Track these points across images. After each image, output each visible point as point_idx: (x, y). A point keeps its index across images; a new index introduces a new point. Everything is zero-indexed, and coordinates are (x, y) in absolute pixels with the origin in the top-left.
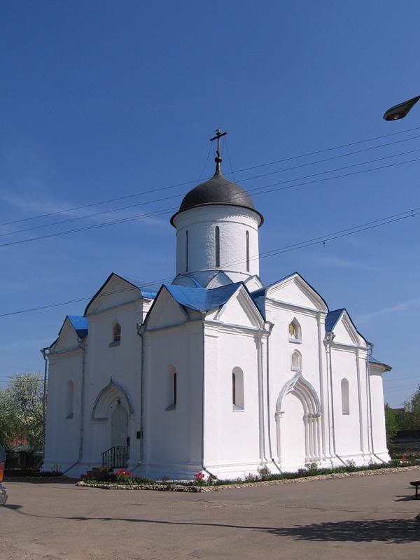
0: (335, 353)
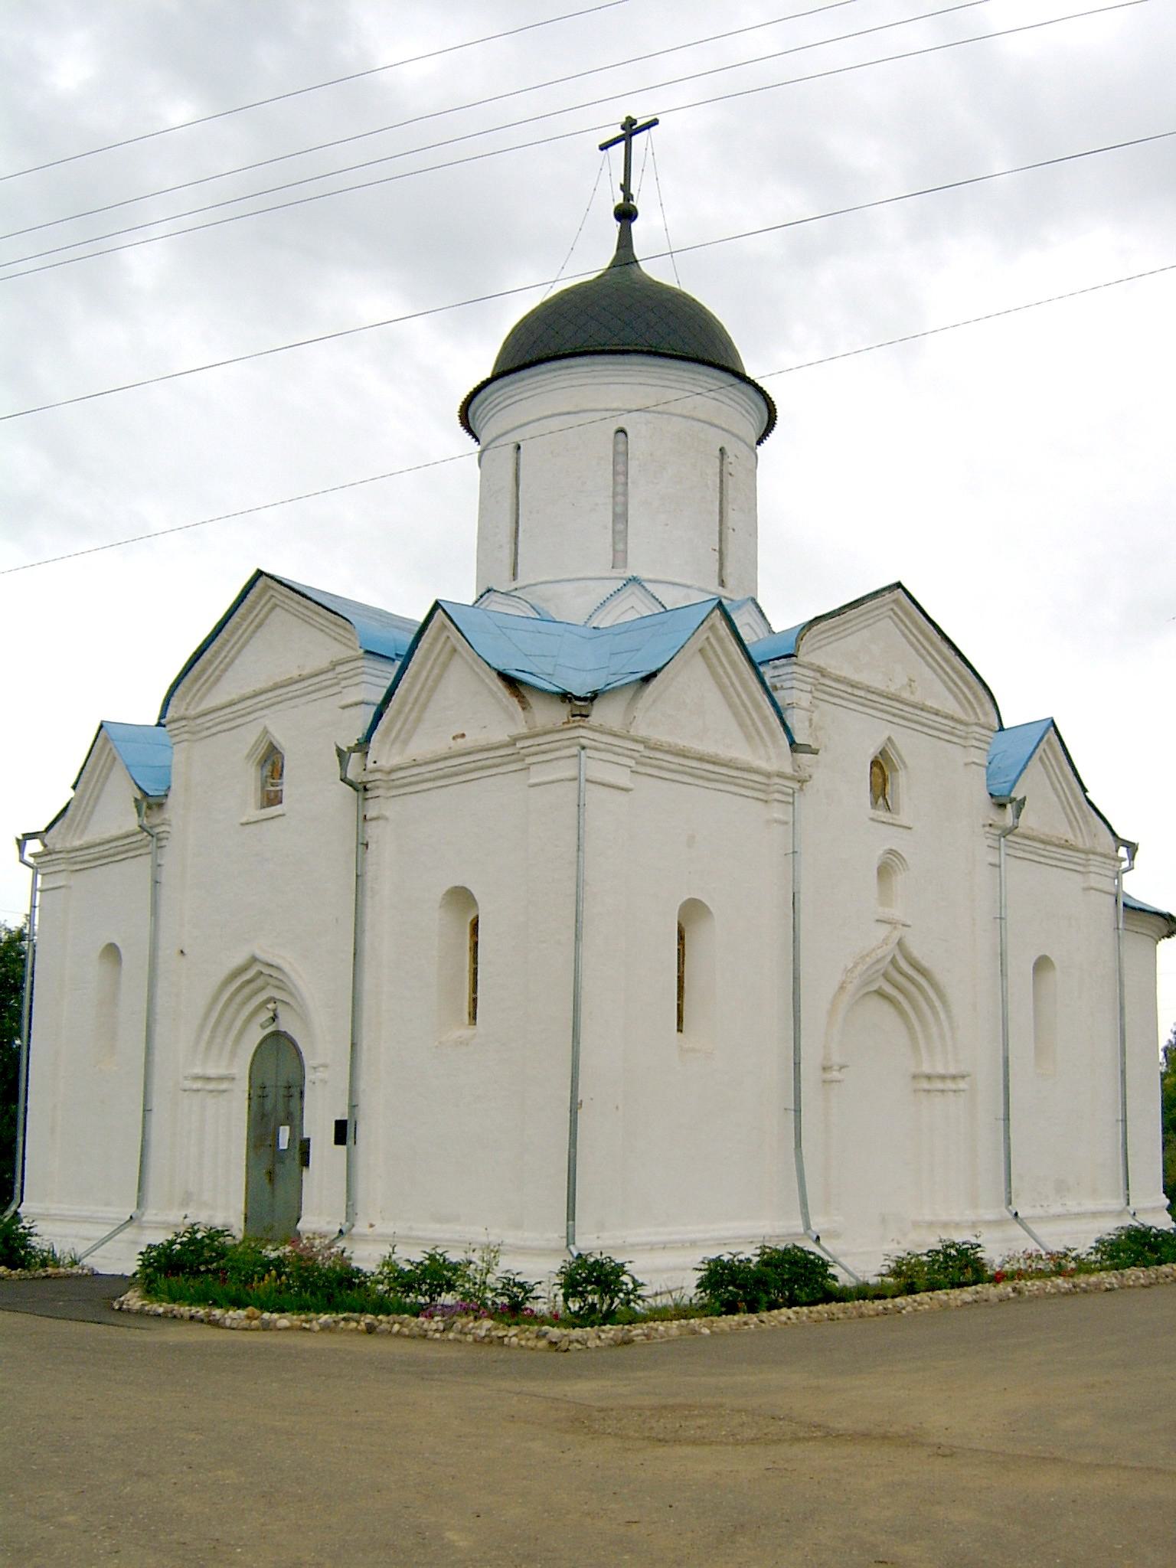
0: (1022, 875)
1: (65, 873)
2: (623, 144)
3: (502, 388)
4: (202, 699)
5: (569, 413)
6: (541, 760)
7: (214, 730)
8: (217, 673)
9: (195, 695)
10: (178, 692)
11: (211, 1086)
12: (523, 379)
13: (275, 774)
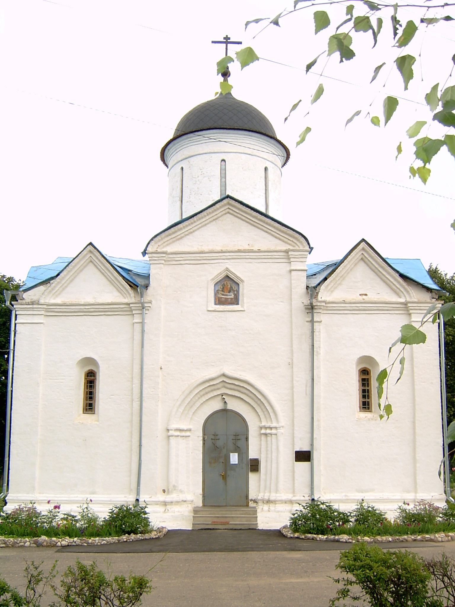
1: (43, 316)
4: (166, 246)
5: (249, 154)
6: (419, 312)
8: (183, 235)
9: (164, 242)
10: (156, 239)
11: (183, 434)
13: (225, 289)
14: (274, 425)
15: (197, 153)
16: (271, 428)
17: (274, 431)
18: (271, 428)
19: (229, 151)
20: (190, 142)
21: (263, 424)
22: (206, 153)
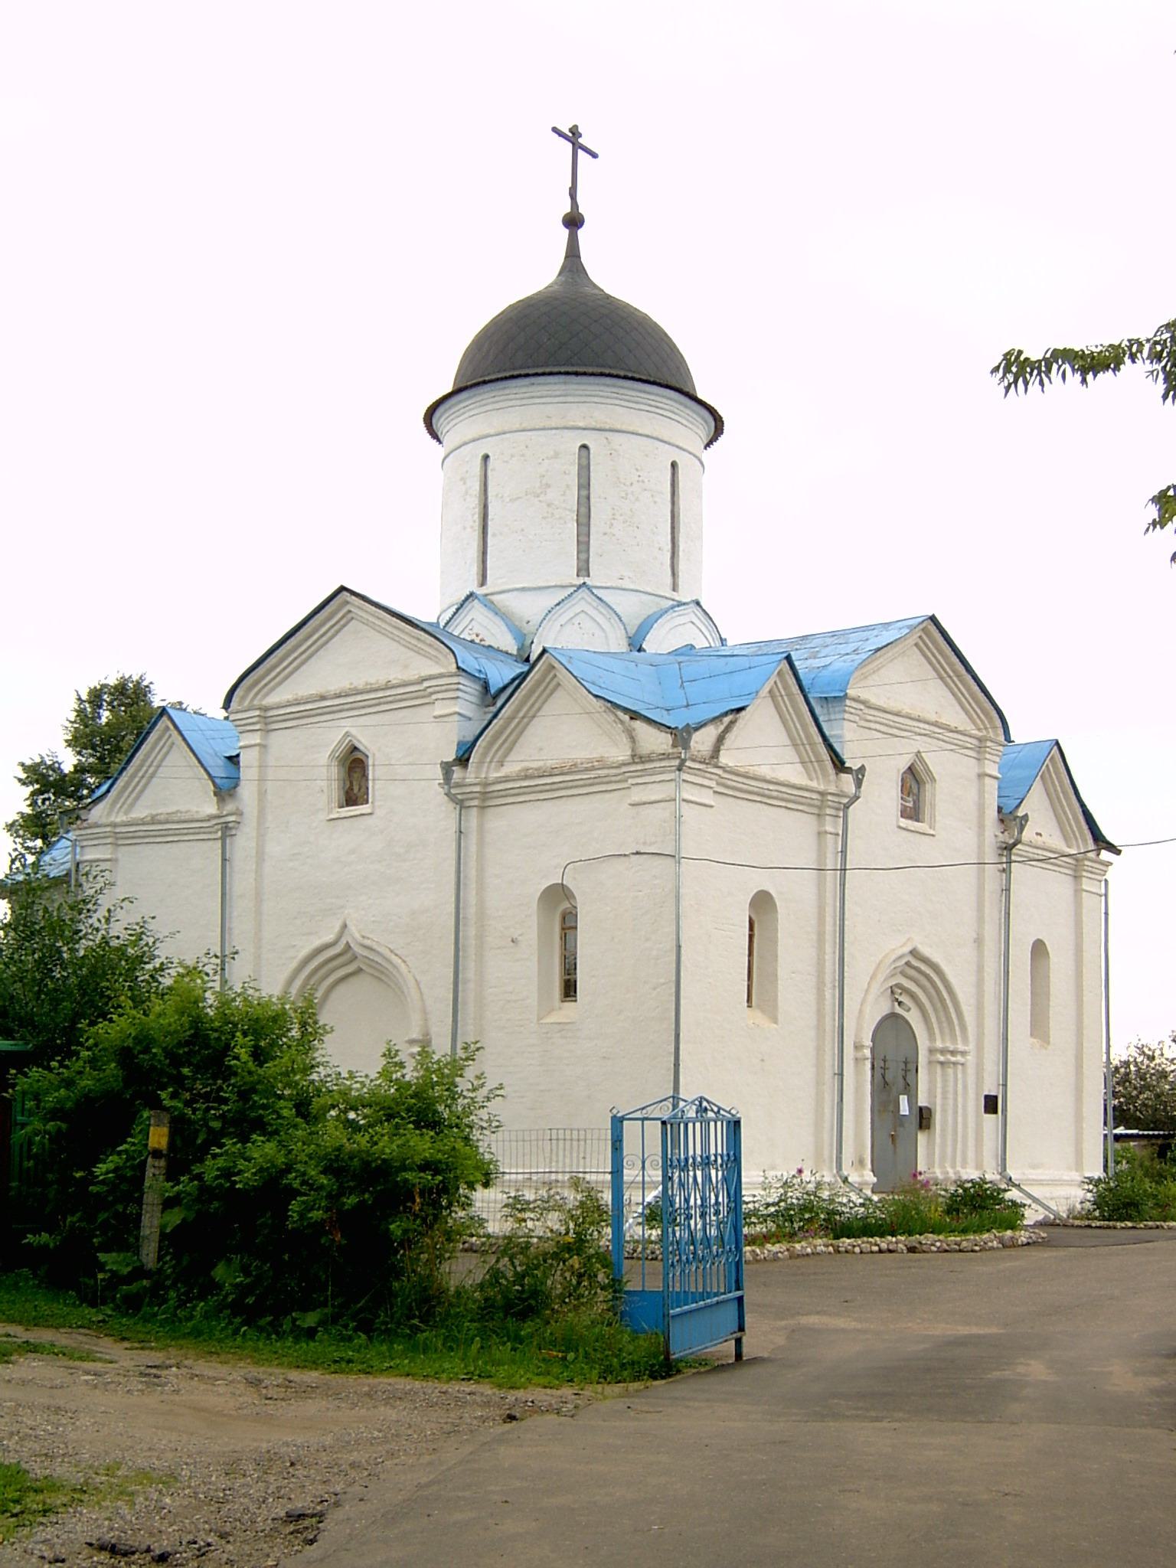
2: (580, 152)
3: (671, 399)
7: (872, 725)
12: (686, 407)
14: (961, 1047)
15: (631, 429)
16: (953, 1053)
17: (959, 1058)
18: (953, 1053)
19: (685, 447)
20: (616, 395)
21: (939, 1044)
22: (647, 436)
